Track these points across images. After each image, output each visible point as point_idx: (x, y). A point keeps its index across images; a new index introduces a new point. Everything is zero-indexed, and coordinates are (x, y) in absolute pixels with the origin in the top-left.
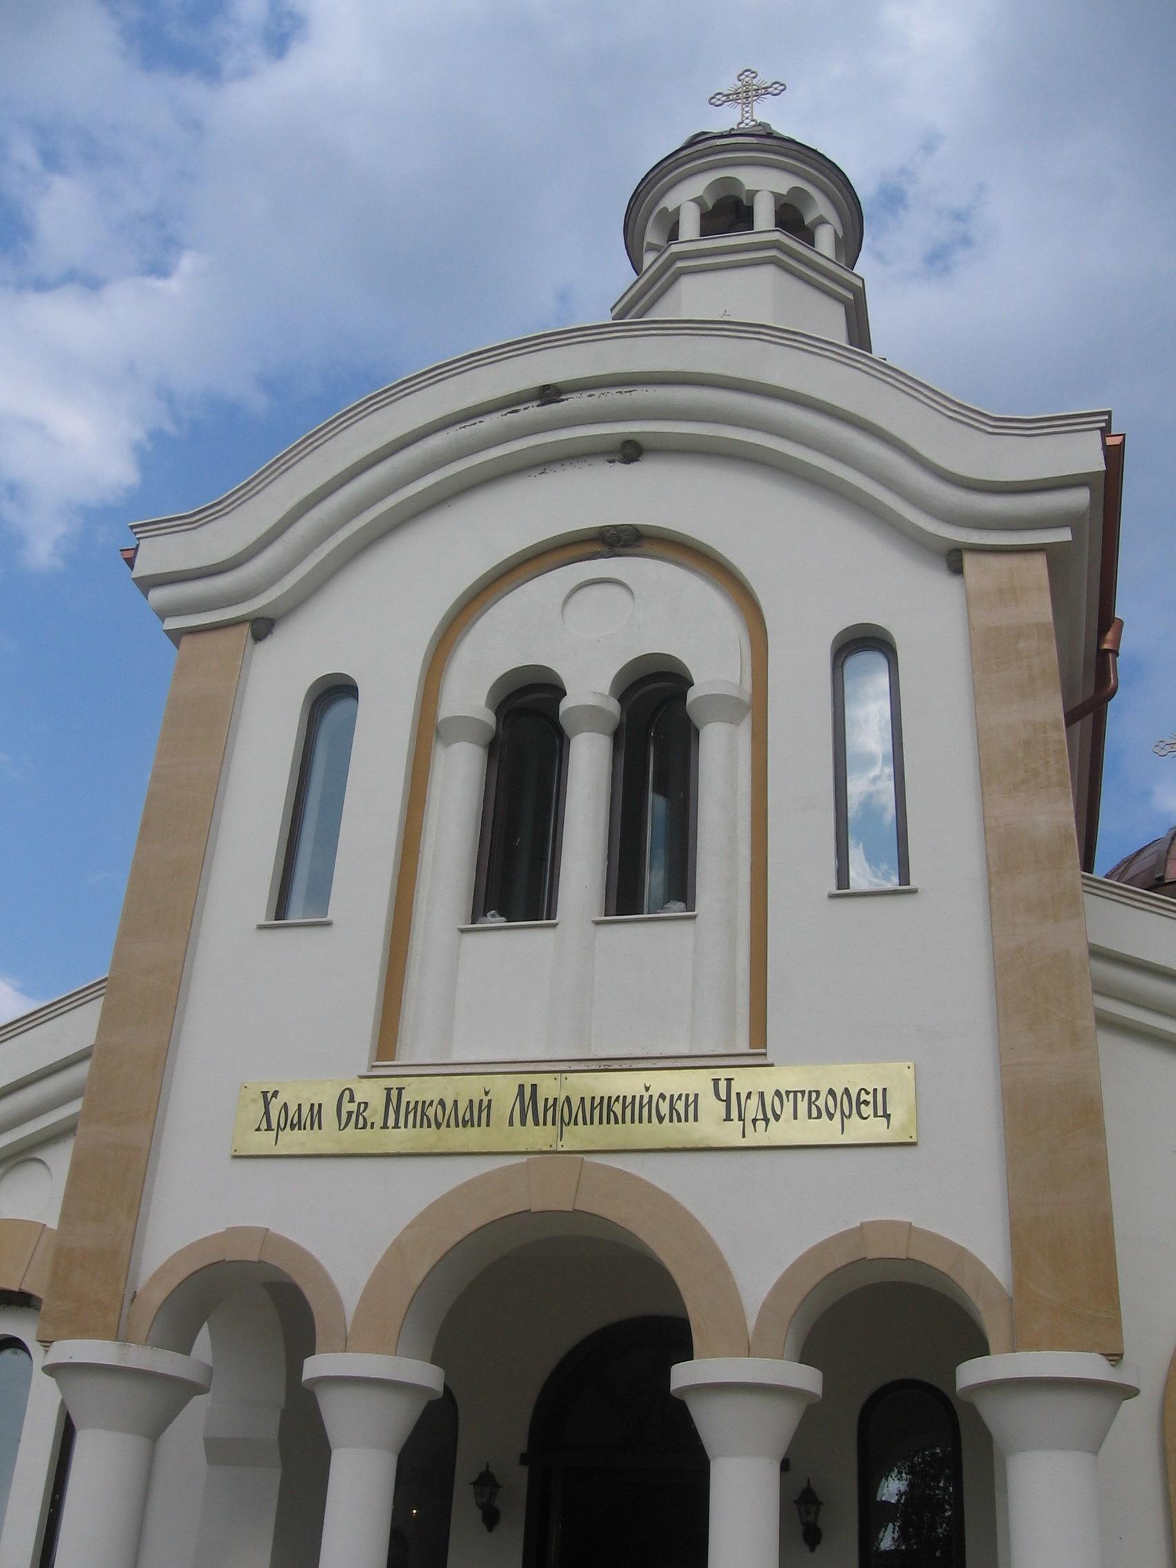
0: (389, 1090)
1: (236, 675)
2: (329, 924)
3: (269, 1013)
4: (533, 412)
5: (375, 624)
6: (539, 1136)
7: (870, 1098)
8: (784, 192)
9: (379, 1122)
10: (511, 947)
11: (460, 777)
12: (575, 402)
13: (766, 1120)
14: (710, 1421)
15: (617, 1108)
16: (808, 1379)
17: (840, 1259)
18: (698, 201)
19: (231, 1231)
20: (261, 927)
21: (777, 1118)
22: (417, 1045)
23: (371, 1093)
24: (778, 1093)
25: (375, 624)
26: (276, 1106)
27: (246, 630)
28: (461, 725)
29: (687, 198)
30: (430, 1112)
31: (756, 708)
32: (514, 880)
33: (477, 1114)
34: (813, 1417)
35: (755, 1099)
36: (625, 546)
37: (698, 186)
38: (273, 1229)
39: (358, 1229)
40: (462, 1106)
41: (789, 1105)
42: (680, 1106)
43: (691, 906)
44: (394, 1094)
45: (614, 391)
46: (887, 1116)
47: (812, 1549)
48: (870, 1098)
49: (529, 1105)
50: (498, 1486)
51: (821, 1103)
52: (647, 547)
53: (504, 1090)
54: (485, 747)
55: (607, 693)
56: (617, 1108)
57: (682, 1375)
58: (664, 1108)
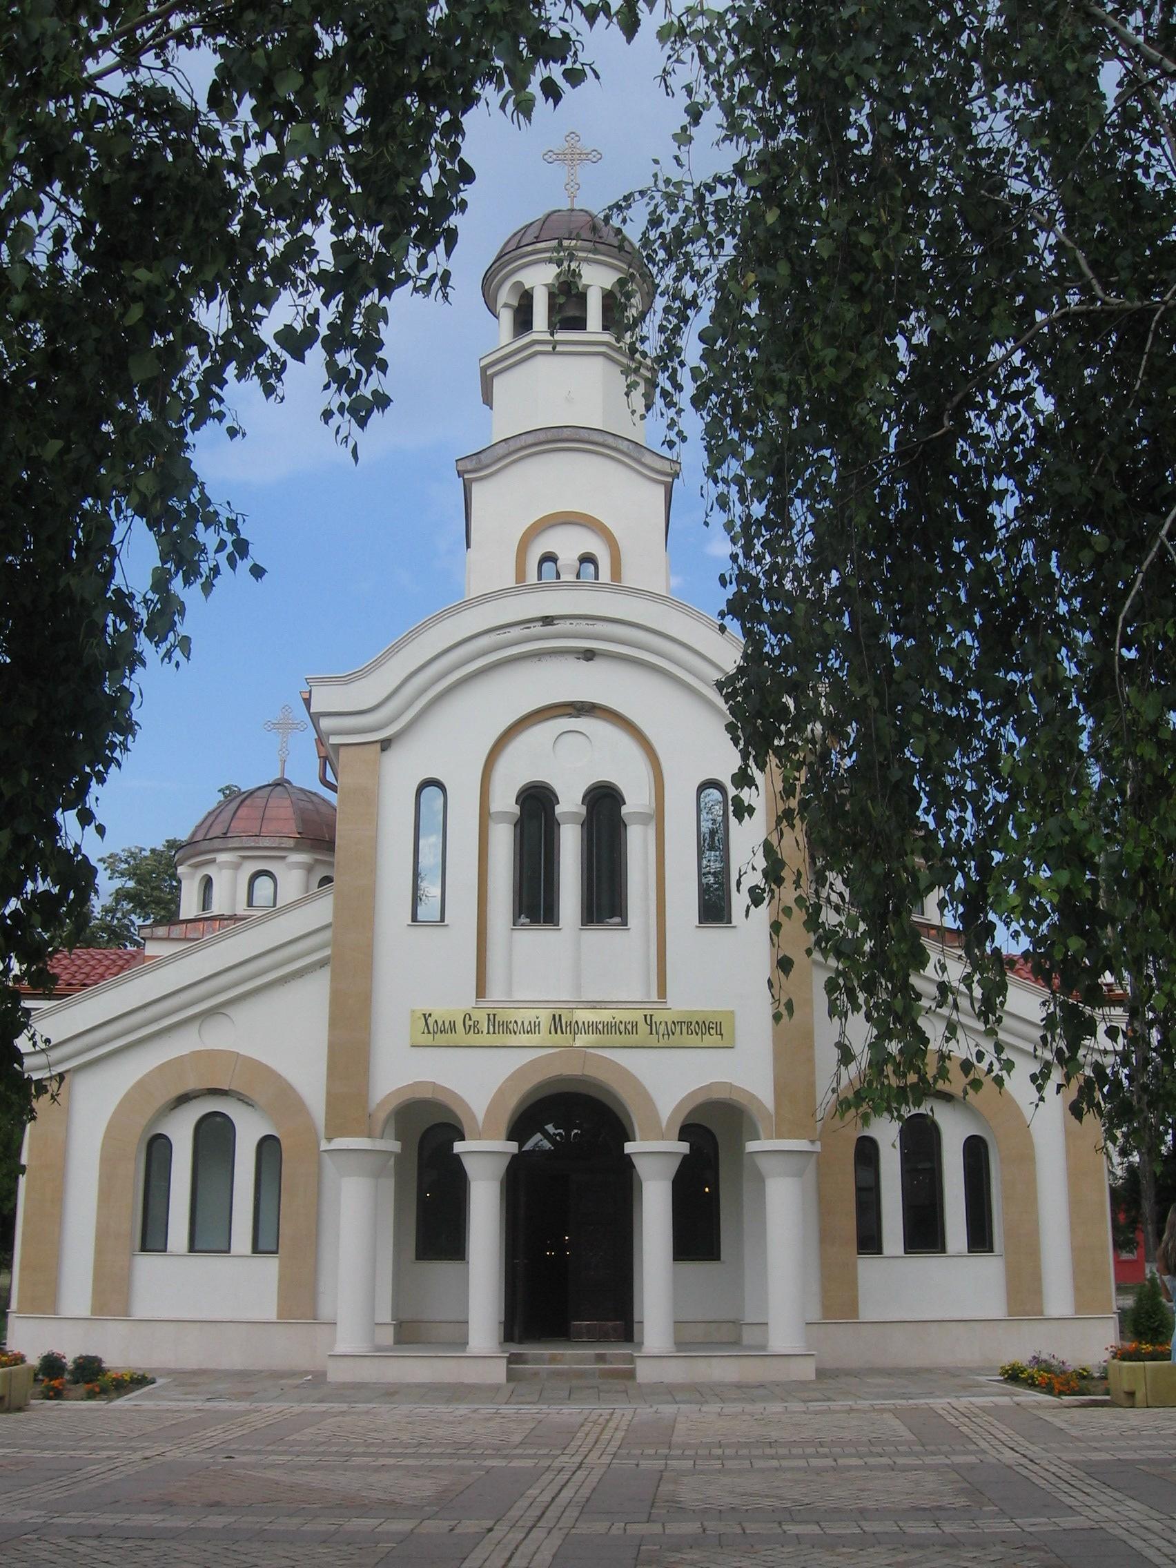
1: (375, 772)
3: (420, 971)
4: (538, 629)
5: (451, 746)
6: (559, 1038)
10: (534, 939)
11: (503, 840)
12: (562, 626)
14: (470, 1165)
15: (600, 1027)
16: (684, 1148)
17: (700, 1099)
19: (417, 1083)
22: (496, 991)
23: (481, 1016)
25: (451, 746)
26: (431, 1021)
27: (378, 746)
28: (504, 815)
30: (511, 1026)
31: (658, 816)
32: (535, 904)
33: (534, 1028)
34: (399, 1159)
39: (481, 1085)
40: (526, 1024)
41: (678, 1029)
42: (629, 1027)
43: (624, 923)
53: (545, 1017)
56: (600, 1027)
57: (629, 1148)
58: (622, 1028)
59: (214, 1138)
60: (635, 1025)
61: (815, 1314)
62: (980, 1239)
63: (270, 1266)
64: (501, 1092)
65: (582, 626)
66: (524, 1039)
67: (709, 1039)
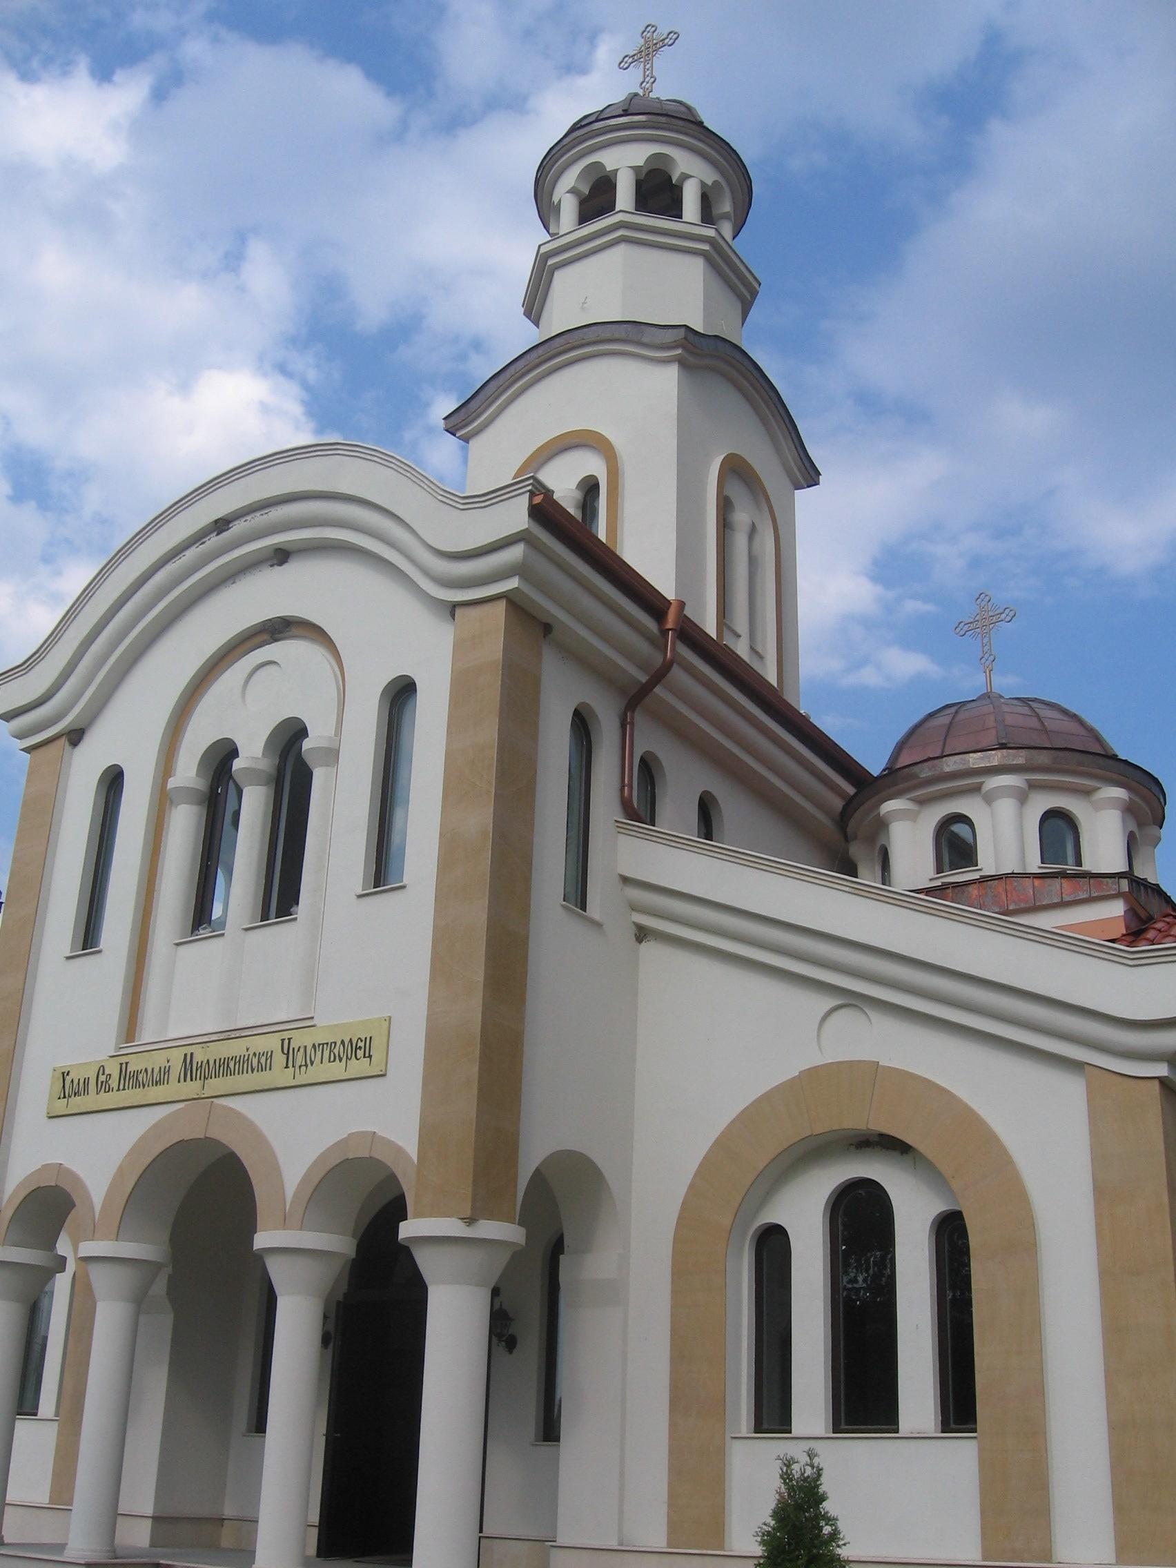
0: (283, 1040)
2: (403, 887)
4: (214, 541)
6: (192, 1088)
7: (362, 1044)
8: (641, 164)
9: (116, 1088)
10: (207, 954)
12: (238, 528)
13: (306, 1065)
18: (573, 191)
20: (68, 958)
21: (312, 1063)
22: (148, 1033)
24: (314, 1046)
26: (68, 1079)
27: (63, 740)
29: (624, 161)
33: (161, 1078)
35: (302, 1050)
36: (280, 632)
37: (570, 179)
38: (380, 1133)
41: (319, 1054)
42: (263, 1060)
44: (286, 1042)
45: (258, 514)
46: (370, 1056)
47: (511, 1352)
48: (362, 1044)
49: (190, 1069)
50: (510, 1319)
51: (336, 1051)
52: (294, 631)
54: (200, 803)
55: (260, 755)
58: (255, 1061)
59: (861, 1223)
60: (270, 1056)
61: (312, 1549)
62: (958, 1408)
63: (962, 1454)
64: (120, 1172)
65: (258, 519)
66: (154, 1093)
67: (358, 1066)
